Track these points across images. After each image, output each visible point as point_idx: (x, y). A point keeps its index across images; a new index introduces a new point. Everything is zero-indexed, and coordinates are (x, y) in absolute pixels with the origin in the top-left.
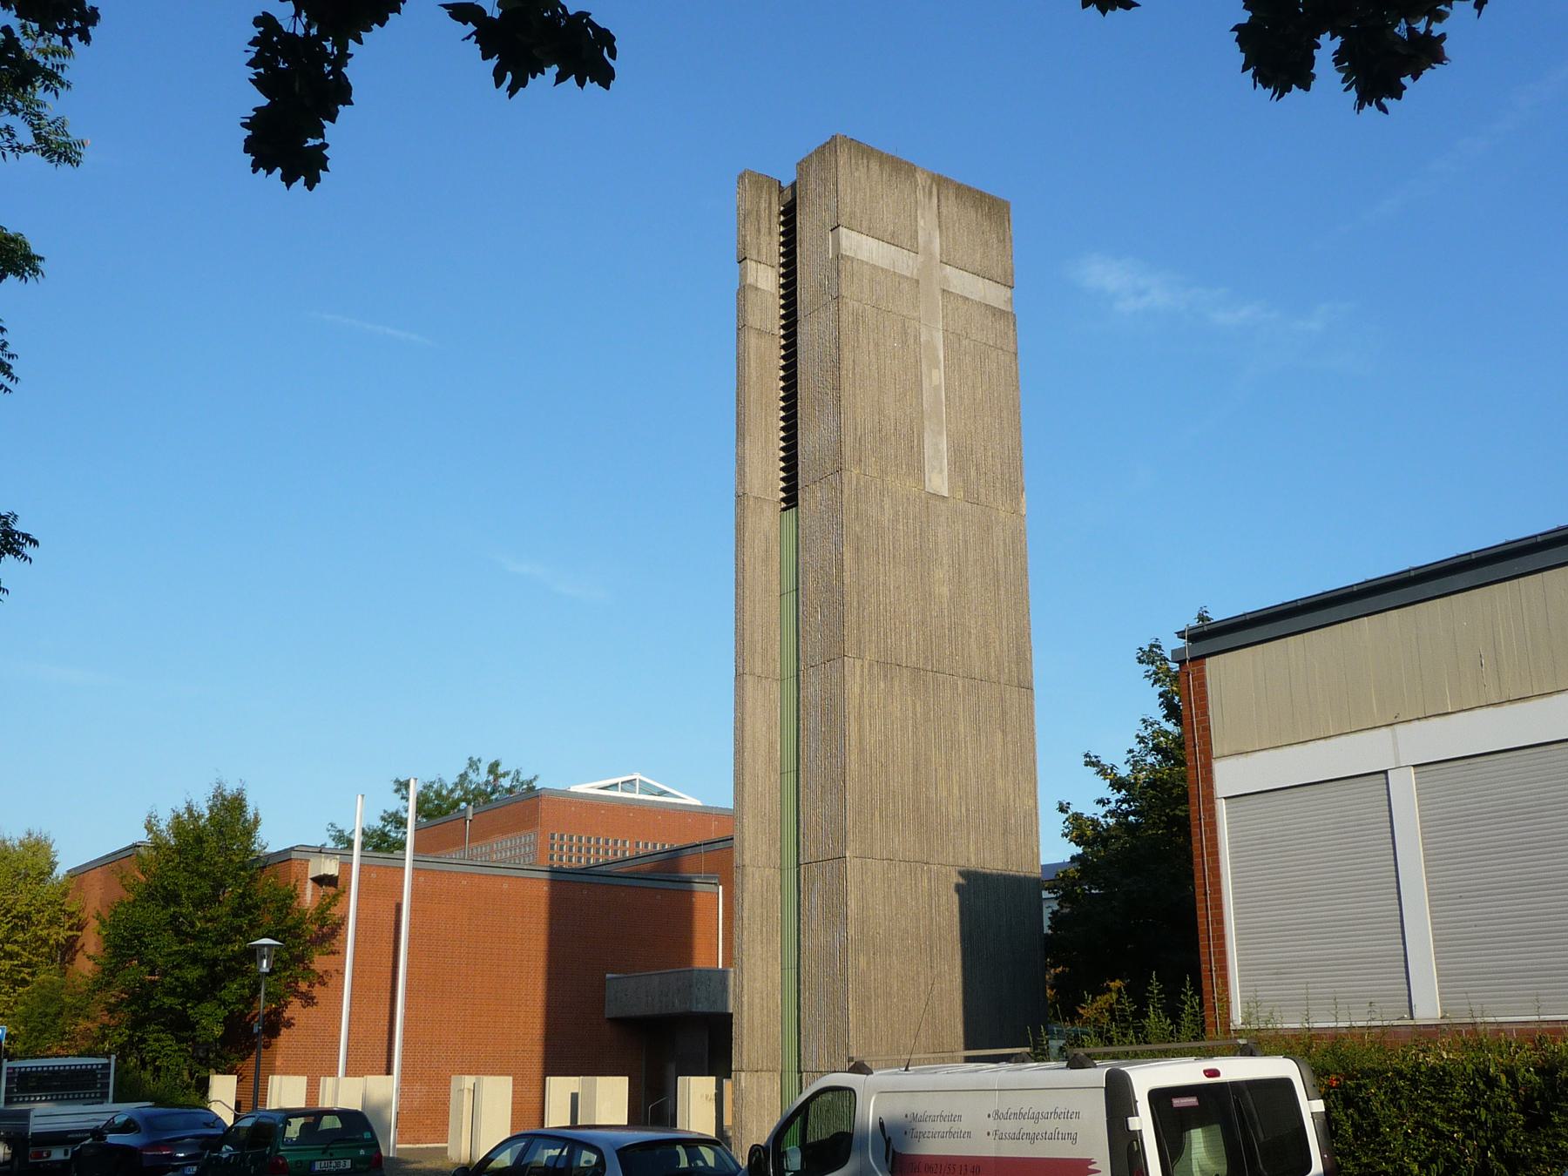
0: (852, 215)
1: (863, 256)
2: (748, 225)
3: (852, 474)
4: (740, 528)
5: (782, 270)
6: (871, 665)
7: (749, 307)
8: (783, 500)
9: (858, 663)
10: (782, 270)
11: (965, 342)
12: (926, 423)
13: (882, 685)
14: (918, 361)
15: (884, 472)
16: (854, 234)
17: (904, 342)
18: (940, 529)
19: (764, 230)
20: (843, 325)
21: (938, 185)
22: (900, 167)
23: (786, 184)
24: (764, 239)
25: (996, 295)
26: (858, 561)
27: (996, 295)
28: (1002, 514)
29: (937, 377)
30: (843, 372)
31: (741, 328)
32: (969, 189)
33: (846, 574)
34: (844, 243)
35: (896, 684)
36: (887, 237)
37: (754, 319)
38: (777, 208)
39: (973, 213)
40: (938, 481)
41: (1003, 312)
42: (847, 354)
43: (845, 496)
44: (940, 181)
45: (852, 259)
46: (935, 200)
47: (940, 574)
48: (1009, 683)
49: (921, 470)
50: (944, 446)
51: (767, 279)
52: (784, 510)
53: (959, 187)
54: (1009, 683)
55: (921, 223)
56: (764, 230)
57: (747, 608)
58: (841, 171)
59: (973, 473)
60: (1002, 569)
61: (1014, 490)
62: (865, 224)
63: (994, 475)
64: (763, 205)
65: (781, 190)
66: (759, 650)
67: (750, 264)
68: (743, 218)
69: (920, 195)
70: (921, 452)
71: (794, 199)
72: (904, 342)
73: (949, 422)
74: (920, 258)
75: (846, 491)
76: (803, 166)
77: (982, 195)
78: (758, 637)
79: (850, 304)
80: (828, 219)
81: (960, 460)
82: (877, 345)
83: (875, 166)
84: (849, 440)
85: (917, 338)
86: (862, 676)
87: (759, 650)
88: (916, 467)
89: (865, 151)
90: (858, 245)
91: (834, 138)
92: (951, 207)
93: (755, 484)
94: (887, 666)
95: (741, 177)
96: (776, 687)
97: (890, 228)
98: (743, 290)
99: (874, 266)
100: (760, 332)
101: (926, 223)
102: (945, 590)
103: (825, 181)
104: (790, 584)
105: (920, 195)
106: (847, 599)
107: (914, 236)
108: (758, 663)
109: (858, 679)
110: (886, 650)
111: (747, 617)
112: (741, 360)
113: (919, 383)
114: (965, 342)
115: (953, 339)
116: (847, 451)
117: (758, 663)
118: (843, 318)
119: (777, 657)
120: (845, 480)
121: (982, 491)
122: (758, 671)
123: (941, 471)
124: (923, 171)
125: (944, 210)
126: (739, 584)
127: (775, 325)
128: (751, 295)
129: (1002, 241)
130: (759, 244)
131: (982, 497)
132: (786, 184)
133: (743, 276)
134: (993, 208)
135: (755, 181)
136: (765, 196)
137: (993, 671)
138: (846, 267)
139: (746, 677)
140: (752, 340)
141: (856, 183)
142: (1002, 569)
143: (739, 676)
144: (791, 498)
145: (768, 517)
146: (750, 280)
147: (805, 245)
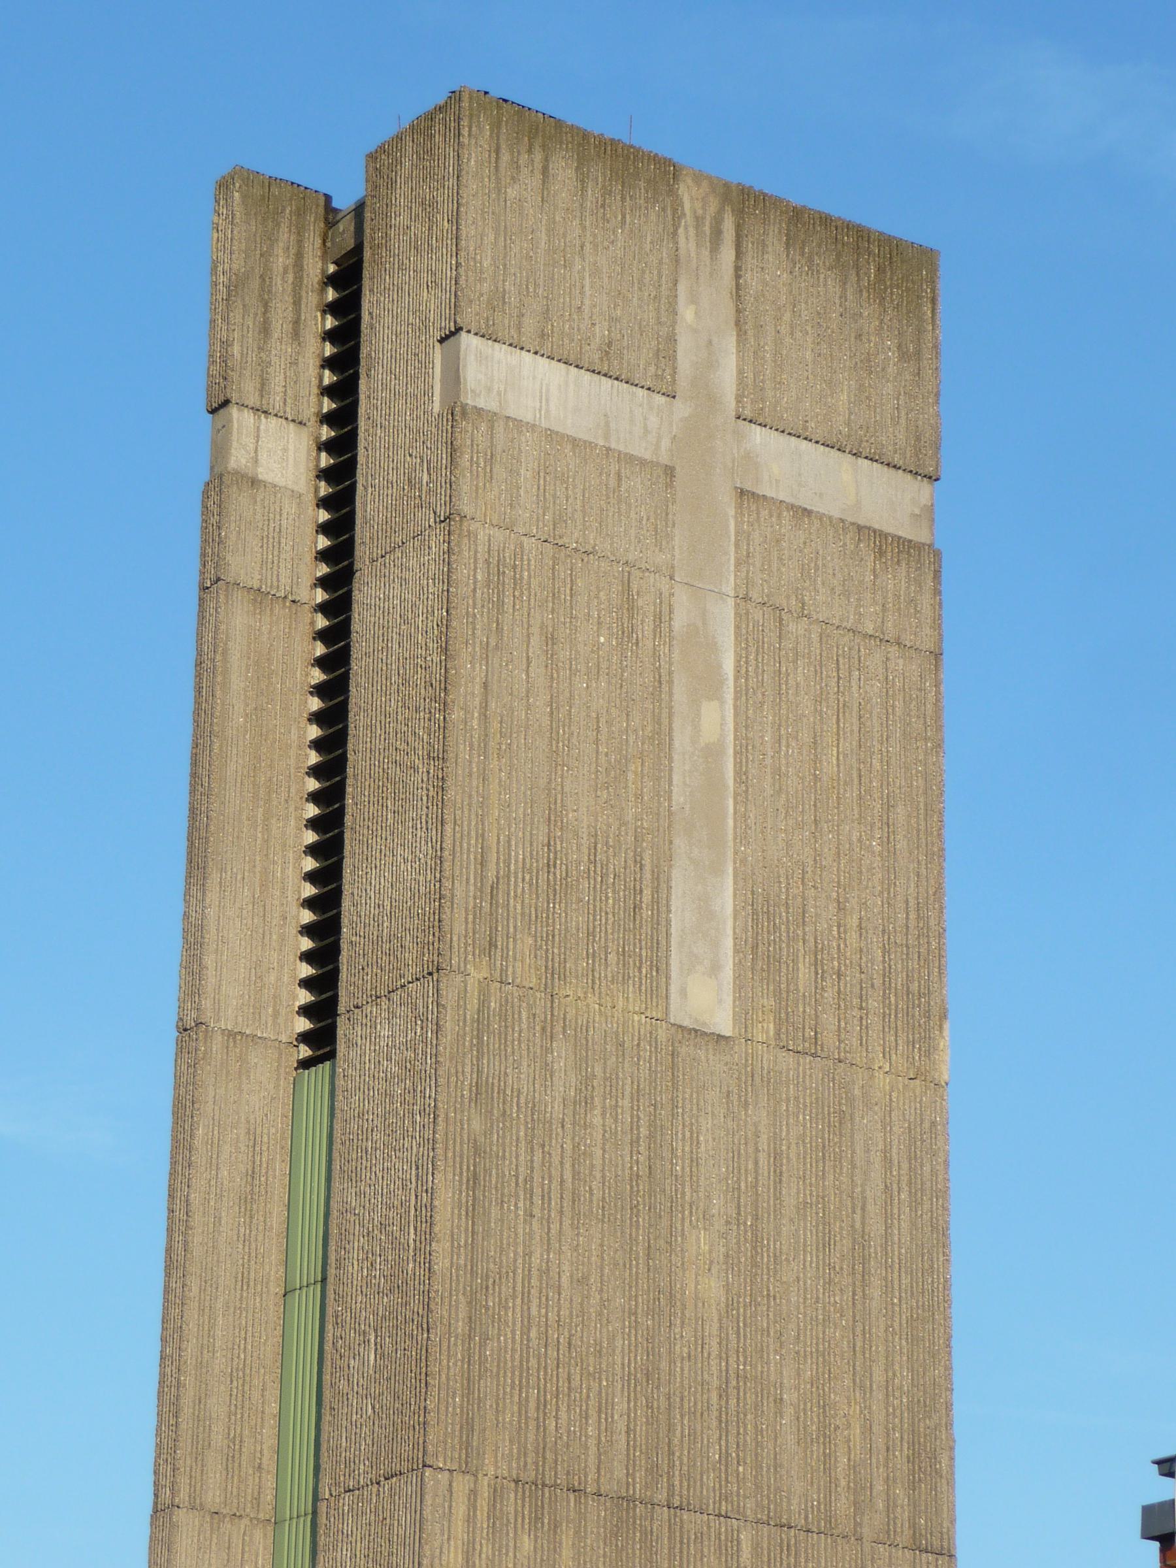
0: (498, 300)
1: (523, 408)
2: (236, 316)
3: (469, 977)
4: (184, 1110)
5: (326, 433)
6: (496, 1494)
7: (230, 532)
8: (305, 1038)
9: (462, 1484)
10: (326, 433)
11: (796, 628)
12: (680, 843)
13: (526, 1543)
14: (661, 683)
15: (554, 973)
16: (500, 352)
17: (628, 635)
18: (706, 1123)
19: (280, 324)
20: (462, 590)
21: (740, 214)
22: (630, 170)
23: (344, 202)
24: (280, 349)
25: (885, 499)
26: (473, 1211)
27: (885, 499)
28: (882, 1081)
29: (717, 720)
30: (456, 715)
31: (211, 585)
32: (826, 220)
33: (441, 1250)
34: (473, 374)
35: (567, 1540)
36: (592, 355)
37: (243, 565)
38: (317, 267)
39: (831, 285)
40: (706, 995)
41: (906, 547)
42: (469, 672)
43: (447, 1039)
44: (746, 203)
45: (491, 418)
46: (728, 254)
47: (701, 1242)
48: (887, 1539)
49: (659, 967)
50: (726, 900)
51: (283, 455)
52: (305, 1064)
53: (797, 215)
54: (887, 1539)
55: (687, 314)
56: (280, 324)
57: (191, 1328)
58: (471, 186)
59: (804, 973)
60: (876, 1228)
61: (918, 1014)
62: (530, 324)
63: (867, 982)
64: (281, 260)
65: (330, 215)
66: (218, 1438)
67: (240, 419)
68: (228, 293)
69: (687, 242)
70: (660, 922)
71: (358, 249)
72: (628, 635)
73: (741, 838)
74: (682, 409)
75: (449, 1025)
76: (381, 162)
77: (861, 234)
78: (217, 1406)
79: (484, 535)
80: (433, 304)
81: (766, 947)
82: (551, 639)
83: (563, 170)
84: (462, 892)
85: (662, 619)
86: (470, 1520)
87: (218, 1438)
88: (649, 963)
89: (535, 130)
90: (509, 379)
91: (455, 96)
92: (773, 268)
93: (228, 1004)
94: (542, 1491)
95: (224, 185)
96: (261, 1539)
97: (601, 331)
98: (220, 485)
99: (551, 435)
100: (260, 596)
101: (701, 316)
102: (713, 1288)
103: (429, 206)
104: (307, 1266)
105: (687, 242)
106: (440, 1311)
107: (666, 351)
108: (214, 1477)
109: (459, 1528)
110: (541, 1451)
111: (190, 1349)
112: (206, 672)
113: (660, 740)
114: (796, 628)
115: (766, 620)
116: (458, 923)
117: (214, 1477)
118: (462, 572)
119: (269, 1461)
120: (450, 996)
121: (829, 1020)
122: (213, 1497)
123: (715, 969)
124: (698, 177)
125: (751, 279)
126: (175, 1264)
127: (300, 572)
128: (239, 502)
129: (911, 355)
130: (264, 365)
131: (829, 1039)
132: (344, 202)
133: (219, 449)
134: (892, 271)
135: (261, 196)
136: (285, 236)
137: (842, 1505)
138: (473, 435)
139: (180, 1516)
140: (238, 618)
141: (510, 216)
142: (876, 1228)
143: (161, 1511)
144: (321, 1041)
145: (262, 1085)
146: (238, 459)
147: (379, 373)
